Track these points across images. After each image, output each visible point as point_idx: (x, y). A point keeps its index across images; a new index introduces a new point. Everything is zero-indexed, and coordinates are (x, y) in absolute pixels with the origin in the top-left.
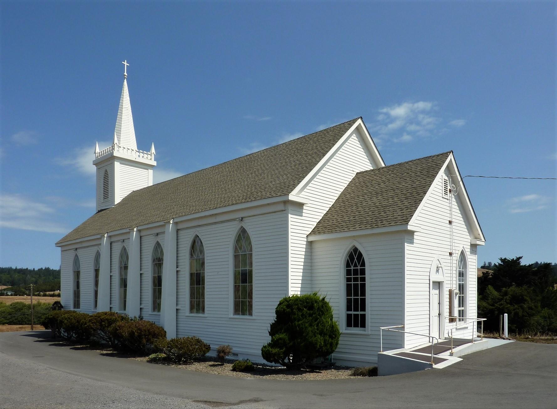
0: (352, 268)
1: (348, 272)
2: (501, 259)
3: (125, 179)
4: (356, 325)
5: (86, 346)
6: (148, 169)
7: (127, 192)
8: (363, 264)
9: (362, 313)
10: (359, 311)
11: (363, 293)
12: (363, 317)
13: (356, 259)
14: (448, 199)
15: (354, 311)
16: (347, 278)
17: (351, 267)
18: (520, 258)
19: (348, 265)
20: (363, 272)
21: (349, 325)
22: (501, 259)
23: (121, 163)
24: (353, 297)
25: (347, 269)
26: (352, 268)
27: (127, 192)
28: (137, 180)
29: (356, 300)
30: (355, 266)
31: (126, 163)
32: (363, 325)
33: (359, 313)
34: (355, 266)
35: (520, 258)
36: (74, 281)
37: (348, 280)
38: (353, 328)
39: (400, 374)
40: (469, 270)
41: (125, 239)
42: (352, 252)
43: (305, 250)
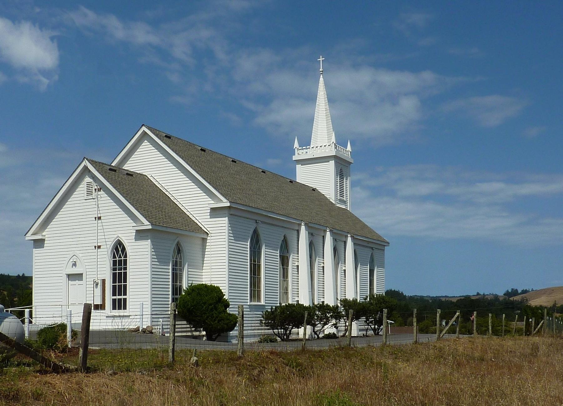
2: (402, 292)
3: (327, 173)
4: (120, 308)
6: (329, 162)
7: (57, 223)
10: (122, 295)
14: (94, 199)
18: (76, 267)
22: (402, 292)
23: (302, 165)
24: (117, 284)
27: (57, 223)
28: (305, 177)
29: (120, 287)
30: (120, 257)
31: (314, 162)
33: (117, 297)
34: (120, 257)
35: (76, 267)
37: (114, 269)
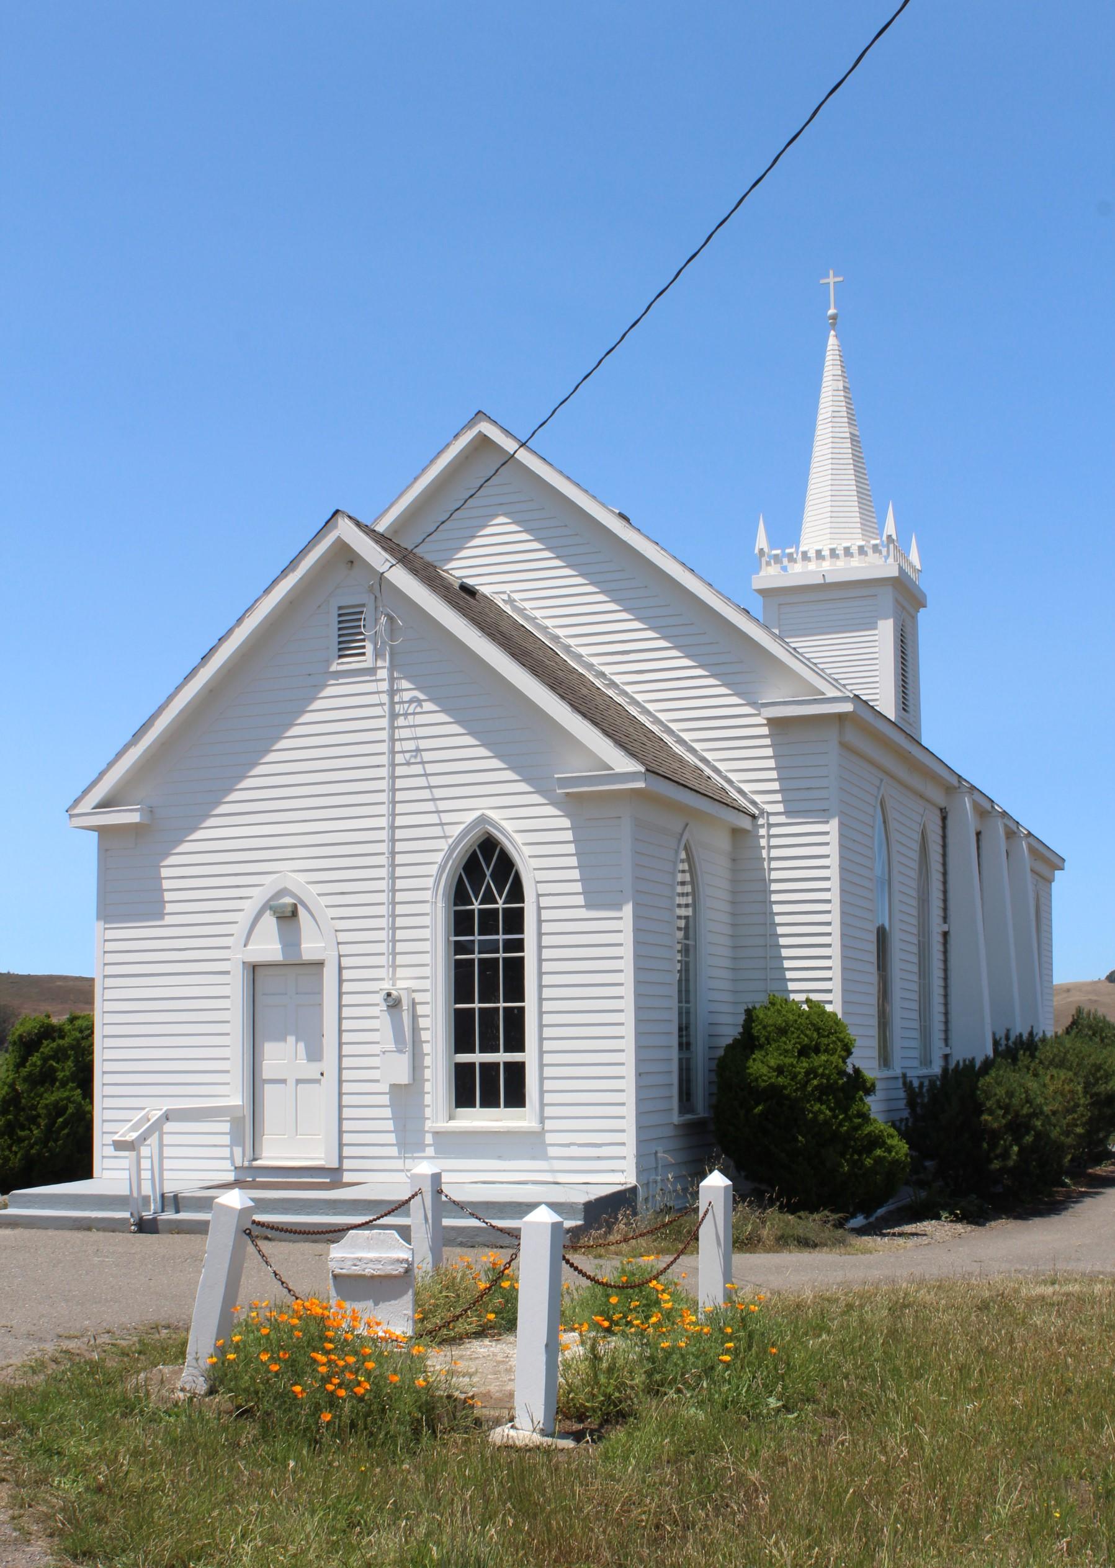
0: (476, 906)
1: (461, 923)
4: (490, 1101)
5: (68, 1112)
8: (517, 893)
9: (464, 1058)
11: (516, 991)
12: (516, 1072)
13: (491, 876)
15: (507, 1050)
16: (456, 942)
17: (497, 903)
19: (460, 895)
20: (515, 920)
21: (463, 1097)
25: (456, 912)
26: (500, 904)
32: (516, 1098)
34: (489, 898)
36: (213, 655)
38: (478, 1111)
39: (379, 1276)
40: (435, 984)
41: (343, 513)
42: (475, 850)
43: (161, 884)
